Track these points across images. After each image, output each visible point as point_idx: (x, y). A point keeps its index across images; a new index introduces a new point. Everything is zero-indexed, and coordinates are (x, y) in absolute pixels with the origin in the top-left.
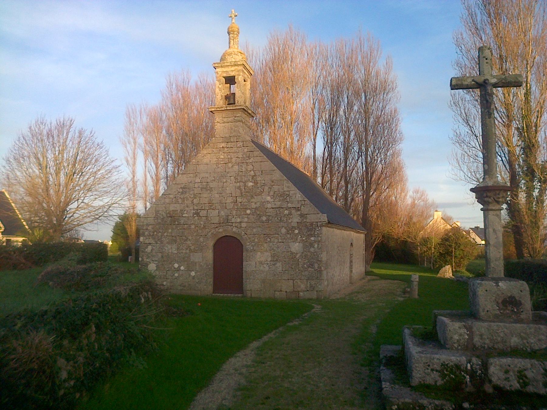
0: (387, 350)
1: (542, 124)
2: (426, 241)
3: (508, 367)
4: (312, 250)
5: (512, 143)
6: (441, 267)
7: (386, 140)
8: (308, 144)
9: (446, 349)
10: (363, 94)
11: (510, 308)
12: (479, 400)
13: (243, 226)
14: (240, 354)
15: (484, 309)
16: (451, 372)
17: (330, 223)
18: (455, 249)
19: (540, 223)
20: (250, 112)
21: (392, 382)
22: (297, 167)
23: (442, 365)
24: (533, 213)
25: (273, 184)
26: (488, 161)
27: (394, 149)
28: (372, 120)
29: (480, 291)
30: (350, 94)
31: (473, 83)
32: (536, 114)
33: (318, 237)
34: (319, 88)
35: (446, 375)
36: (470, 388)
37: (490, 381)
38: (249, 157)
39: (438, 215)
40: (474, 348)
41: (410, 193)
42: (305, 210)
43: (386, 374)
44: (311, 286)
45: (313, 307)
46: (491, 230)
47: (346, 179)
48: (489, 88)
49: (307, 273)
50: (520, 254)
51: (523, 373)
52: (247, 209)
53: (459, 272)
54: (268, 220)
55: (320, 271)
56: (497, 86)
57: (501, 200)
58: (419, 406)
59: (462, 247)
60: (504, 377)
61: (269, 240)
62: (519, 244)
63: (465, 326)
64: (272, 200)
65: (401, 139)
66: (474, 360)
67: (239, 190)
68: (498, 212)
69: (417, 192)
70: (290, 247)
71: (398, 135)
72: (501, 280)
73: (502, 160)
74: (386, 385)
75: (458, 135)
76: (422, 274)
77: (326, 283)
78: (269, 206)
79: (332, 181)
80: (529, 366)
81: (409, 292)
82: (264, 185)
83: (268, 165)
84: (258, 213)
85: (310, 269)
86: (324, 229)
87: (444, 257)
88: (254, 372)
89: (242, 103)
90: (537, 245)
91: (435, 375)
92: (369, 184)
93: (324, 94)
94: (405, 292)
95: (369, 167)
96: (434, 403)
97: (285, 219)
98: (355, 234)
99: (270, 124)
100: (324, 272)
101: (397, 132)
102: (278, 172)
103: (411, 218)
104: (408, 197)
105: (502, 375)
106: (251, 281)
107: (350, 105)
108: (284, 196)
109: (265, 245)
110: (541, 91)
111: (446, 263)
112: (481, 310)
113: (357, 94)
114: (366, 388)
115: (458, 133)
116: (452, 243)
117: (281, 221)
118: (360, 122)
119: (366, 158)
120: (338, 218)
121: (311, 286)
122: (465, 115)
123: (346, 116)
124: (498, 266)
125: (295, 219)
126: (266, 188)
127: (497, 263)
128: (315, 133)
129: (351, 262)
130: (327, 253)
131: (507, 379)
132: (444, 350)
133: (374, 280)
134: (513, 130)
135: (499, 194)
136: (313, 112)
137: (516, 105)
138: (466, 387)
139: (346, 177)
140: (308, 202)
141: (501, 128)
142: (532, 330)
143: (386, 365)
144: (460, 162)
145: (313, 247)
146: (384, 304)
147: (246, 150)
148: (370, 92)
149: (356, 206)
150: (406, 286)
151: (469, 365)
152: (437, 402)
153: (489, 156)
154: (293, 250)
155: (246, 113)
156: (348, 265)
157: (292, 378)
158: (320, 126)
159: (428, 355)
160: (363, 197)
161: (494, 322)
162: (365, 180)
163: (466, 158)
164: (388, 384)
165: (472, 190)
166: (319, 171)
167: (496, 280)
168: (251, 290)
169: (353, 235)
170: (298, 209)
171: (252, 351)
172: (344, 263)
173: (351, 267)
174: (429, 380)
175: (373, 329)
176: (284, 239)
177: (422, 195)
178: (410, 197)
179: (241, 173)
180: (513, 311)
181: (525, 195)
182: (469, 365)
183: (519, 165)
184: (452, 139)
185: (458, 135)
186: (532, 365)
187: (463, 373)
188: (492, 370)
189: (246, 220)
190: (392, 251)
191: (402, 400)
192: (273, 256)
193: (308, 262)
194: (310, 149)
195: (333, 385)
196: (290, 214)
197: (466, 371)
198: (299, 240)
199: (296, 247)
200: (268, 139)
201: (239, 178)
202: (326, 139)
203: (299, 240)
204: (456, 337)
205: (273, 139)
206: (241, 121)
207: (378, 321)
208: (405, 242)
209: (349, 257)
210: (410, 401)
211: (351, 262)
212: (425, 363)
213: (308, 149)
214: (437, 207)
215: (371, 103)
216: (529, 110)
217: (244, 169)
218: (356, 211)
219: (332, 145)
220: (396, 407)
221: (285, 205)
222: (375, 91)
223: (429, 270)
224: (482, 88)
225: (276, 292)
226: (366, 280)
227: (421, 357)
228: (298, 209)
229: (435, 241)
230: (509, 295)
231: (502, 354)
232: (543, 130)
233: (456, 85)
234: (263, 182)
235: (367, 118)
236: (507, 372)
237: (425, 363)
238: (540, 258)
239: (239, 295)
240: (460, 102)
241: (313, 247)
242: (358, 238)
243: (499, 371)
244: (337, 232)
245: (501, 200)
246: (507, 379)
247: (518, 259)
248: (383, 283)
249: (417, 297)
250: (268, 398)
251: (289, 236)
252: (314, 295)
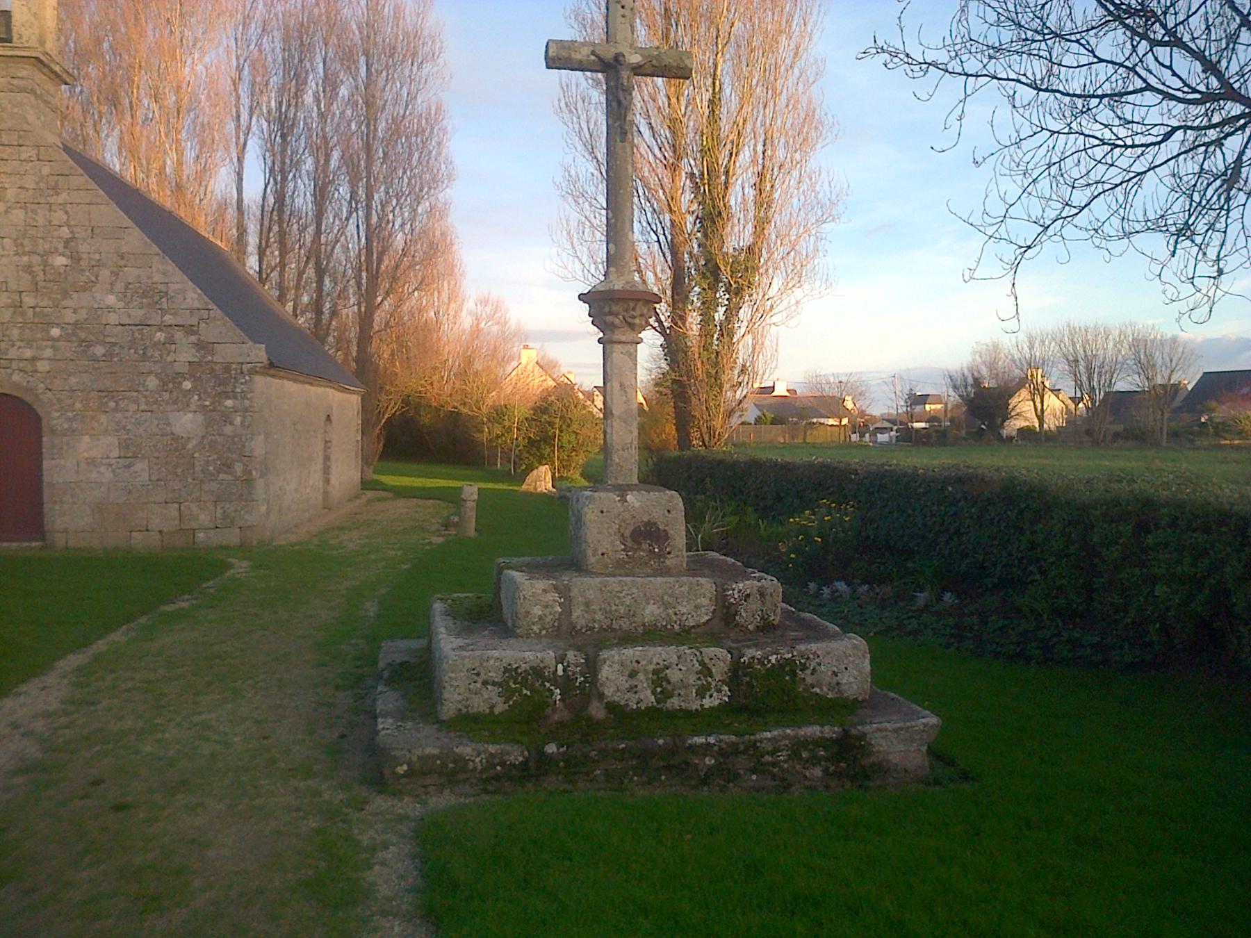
0: (396, 650)
1: (739, 171)
2: (500, 413)
3: (635, 664)
4: (228, 430)
5: (680, 209)
6: (531, 469)
7: (415, 176)
8: (223, 171)
9: (517, 636)
10: (362, 60)
11: (645, 546)
12: (578, 736)
13: (41, 369)
14: (32, 687)
15: (595, 550)
16: (524, 683)
17: (273, 367)
18: (561, 431)
19: (725, 378)
20: (57, 69)
21: (401, 716)
22: (194, 225)
23: (506, 670)
24: (713, 356)
25: (122, 263)
26: (616, 231)
27: (432, 199)
28: (382, 125)
29: (590, 515)
30: (330, 54)
31: (593, 57)
32: (729, 146)
33: (244, 398)
34: (254, 31)
35: (515, 690)
36: (561, 714)
37: (601, 696)
38: (56, 190)
39: (528, 357)
40: (574, 631)
41: (470, 305)
42: (209, 333)
43: (387, 699)
44: (225, 515)
45: (230, 566)
46: (616, 385)
47: (318, 264)
48: (625, 74)
49: (214, 486)
50: (684, 441)
51: (662, 675)
52: (50, 324)
53: (567, 478)
54: (109, 356)
55: (248, 481)
56: (641, 71)
57: (637, 321)
58: (454, 761)
59: (575, 427)
60: (627, 685)
61: (112, 404)
62: (683, 421)
63: (555, 588)
64: (122, 304)
65: (450, 176)
66: (571, 655)
67: (26, 276)
68: (630, 348)
69: (484, 302)
70: (169, 424)
71: (443, 166)
72: (631, 490)
73: (659, 241)
74: (385, 725)
75: (573, 180)
76: (482, 485)
77: (263, 509)
78: (113, 318)
79: (282, 265)
80: (675, 659)
81: (456, 525)
82: (100, 263)
83: (109, 213)
84: (83, 335)
85: (222, 476)
86: (259, 380)
87: (538, 449)
88: (67, 727)
89: (34, 42)
90: (717, 423)
91: (492, 693)
92: (374, 278)
93: (266, 46)
94: (447, 525)
95: (376, 236)
96: (485, 751)
97: (157, 354)
98: (338, 394)
99: (120, 108)
100: (260, 484)
101: (441, 159)
102: (136, 232)
103: (469, 361)
104: (464, 313)
105: (624, 683)
106: (66, 506)
107: (330, 83)
108: (153, 296)
109: (103, 418)
110: (741, 99)
111: (541, 460)
112: (590, 552)
113: (348, 58)
114: (343, 736)
115: (573, 173)
116: (551, 420)
117: (144, 357)
118: (353, 126)
119: (368, 217)
120: (295, 354)
121: (225, 515)
122: (588, 136)
123: (319, 109)
124: (628, 461)
125: (184, 355)
126: (105, 274)
127: (626, 454)
128: (242, 140)
129: (327, 458)
130: (266, 438)
131: (633, 689)
132: (512, 641)
133: (379, 500)
134: (683, 180)
135: (634, 309)
136: (236, 90)
137: (691, 124)
138: (554, 711)
139: (318, 257)
140: (216, 312)
141: (659, 171)
142: (685, 589)
143: (390, 682)
144: (575, 240)
145: (231, 424)
146: (399, 553)
147: (46, 170)
148: (379, 56)
149: (343, 330)
150: (452, 511)
151: (560, 667)
152: (492, 749)
153: (619, 225)
154: (178, 429)
155: (45, 70)
156: (319, 466)
157: (163, 732)
158: (254, 128)
159: (478, 653)
160: (359, 309)
161: (614, 576)
162: (364, 268)
163: (587, 230)
164: (391, 720)
165: (582, 297)
166: (253, 240)
167: (622, 490)
168: (66, 531)
169: (333, 396)
170: (190, 330)
171: (64, 677)
172: (308, 462)
173: (326, 470)
174: (479, 705)
175: (371, 608)
176: (155, 403)
177: (497, 310)
178: (470, 313)
179: (32, 232)
180: (652, 551)
181: (699, 318)
182: (560, 667)
183: (690, 253)
184: (559, 187)
185: (573, 180)
186: (679, 657)
187: (547, 685)
188: (605, 672)
189: (48, 353)
190: (424, 435)
191: (419, 752)
192: (125, 445)
193: (218, 459)
194: (233, 182)
195: (265, 738)
196: (170, 341)
197: (554, 680)
198: (193, 407)
199: (187, 423)
200: (115, 149)
201: (26, 242)
202: (269, 163)
203: (193, 407)
204: (537, 611)
205: (129, 148)
206: (33, 92)
207: (383, 591)
208: (455, 416)
209: (320, 446)
210: (436, 751)
211: (327, 458)
212: (470, 667)
213: (221, 183)
214: (526, 340)
215: (381, 83)
216: (716, 138)
217: (41, 221)
218: (341, 341)
219: (284, 179)
220: (405, 767)
221: (155, 319)
222: (392, 56)
223: (505, 477)
224: (613, 70)
225: (134, 534)
226: (363, 500)
227: (464, 658)
228: (190, 330)
229: (521, 411)
230: (646, 520)
231: (628, 639)
232: (739, 182)
233: (559, 58)
234: (97, 256)
235: (370, 120)
236: (633, 675)
237: (470, 667)
238: (721, 448)
239: (34, 544)
240: (580, 105)
241: (231, 424)
242: (345, 404)
243: (620, 676)
244: (291, 387)
245: (637, 321)
246: (633, 689)
247: (681, 449)
248: (401, 507)
249: (472, 534)
250: (97, 782)
251: (166, 396)
252: (233, 538)
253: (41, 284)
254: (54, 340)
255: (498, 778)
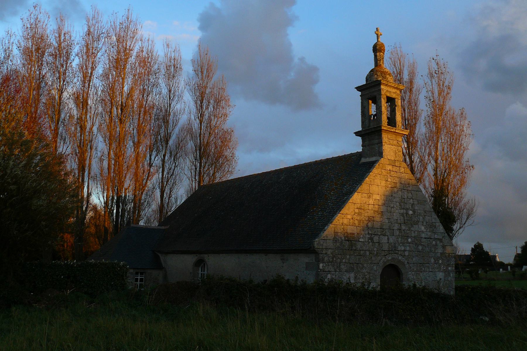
25: (425, 214)
52: (408, 237)
78: (423, 235)
189: (408, 248)
196: (436, 245)
253: (406, 221)
254: (410, 243)
255: (104, 226)
